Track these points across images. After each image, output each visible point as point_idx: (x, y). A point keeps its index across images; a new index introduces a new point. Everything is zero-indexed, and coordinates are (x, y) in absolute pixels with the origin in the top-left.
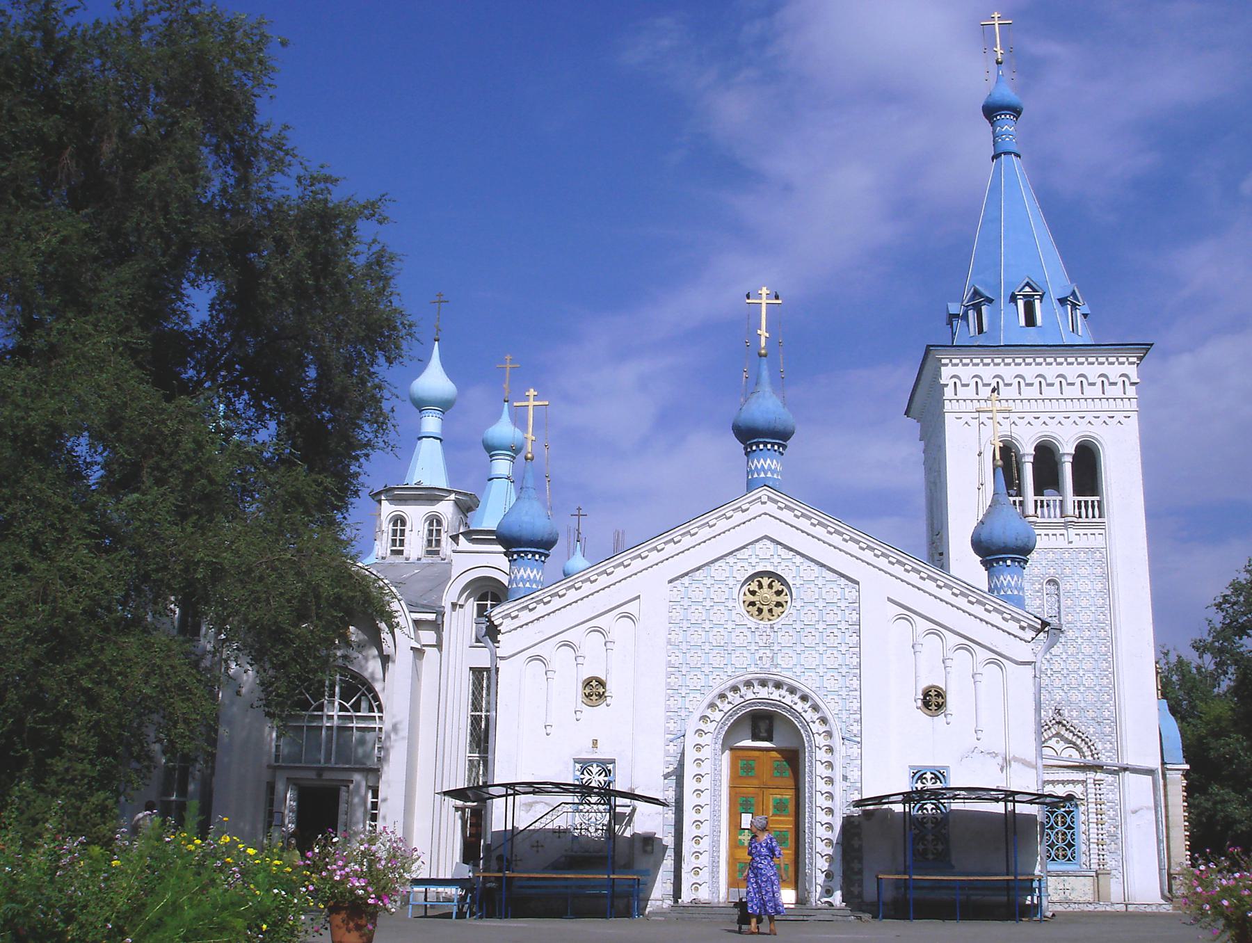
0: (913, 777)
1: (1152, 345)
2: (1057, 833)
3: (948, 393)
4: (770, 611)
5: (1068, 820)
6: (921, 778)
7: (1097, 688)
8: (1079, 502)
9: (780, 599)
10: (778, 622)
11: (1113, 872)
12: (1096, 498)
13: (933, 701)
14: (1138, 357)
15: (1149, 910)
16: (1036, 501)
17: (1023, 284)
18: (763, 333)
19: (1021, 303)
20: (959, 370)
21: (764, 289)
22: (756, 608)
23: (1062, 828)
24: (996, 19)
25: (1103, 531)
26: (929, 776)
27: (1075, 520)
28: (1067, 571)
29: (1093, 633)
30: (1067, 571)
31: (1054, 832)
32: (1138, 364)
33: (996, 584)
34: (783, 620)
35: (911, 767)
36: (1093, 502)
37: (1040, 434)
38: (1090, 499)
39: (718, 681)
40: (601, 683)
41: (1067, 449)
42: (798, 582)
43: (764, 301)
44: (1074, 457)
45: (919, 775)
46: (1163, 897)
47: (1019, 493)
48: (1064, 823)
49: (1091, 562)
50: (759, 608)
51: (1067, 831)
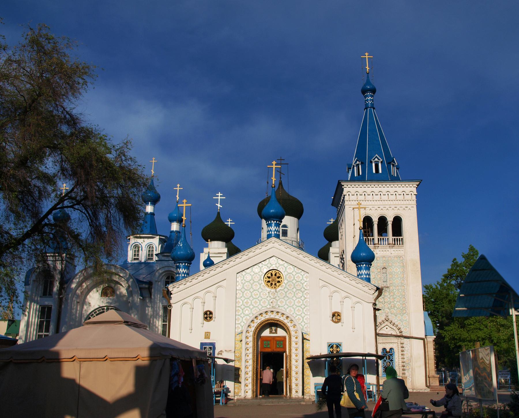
0: (329, 346)
1: (422, 180)
2: (387, 362)
3: (346, 198)
4: (275, 284)
5: (391, 358)
6: (332, 347)
7: (401, 308)
8: (395, 239)
9: (279, 280)
10: (278, 289)
11: (408, 377)
12: (401, 237)
13: (336, 317)
14: (417, 185)
15: (421, 391)
16: (379, 239)
17: (375, 157)
18: (368, 68)
19: (374, 165)
20: (351, 189)
21: (274, 162)
22: (270, 283)
23: (389, 361)
24: (367, 55)
25: (403, 250)
26: (335, 346)
27: (393, 245)
28: (390, 264)
29: (400, 288)
30: (390, 264)
31: (386, 362)
32: (417, 188)
33: (360, 273)
34: (280, 288)
35: (328, 343)
36: (400, 239)
37: (380, 214)
38: (398, 238)
39: (255, 311)
40: (211, 313)
41: (390, 220)
42: (286, 273)
43: (274, 167)
44: (393, 222)
45: (331, 346)
46: (427, 386)
47: (372, 236)
48: (389, 359)
49: (399, 261)
50: (271, 283)
51: (390, 362)
